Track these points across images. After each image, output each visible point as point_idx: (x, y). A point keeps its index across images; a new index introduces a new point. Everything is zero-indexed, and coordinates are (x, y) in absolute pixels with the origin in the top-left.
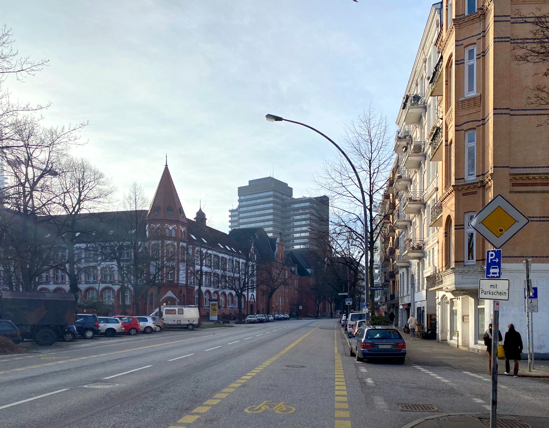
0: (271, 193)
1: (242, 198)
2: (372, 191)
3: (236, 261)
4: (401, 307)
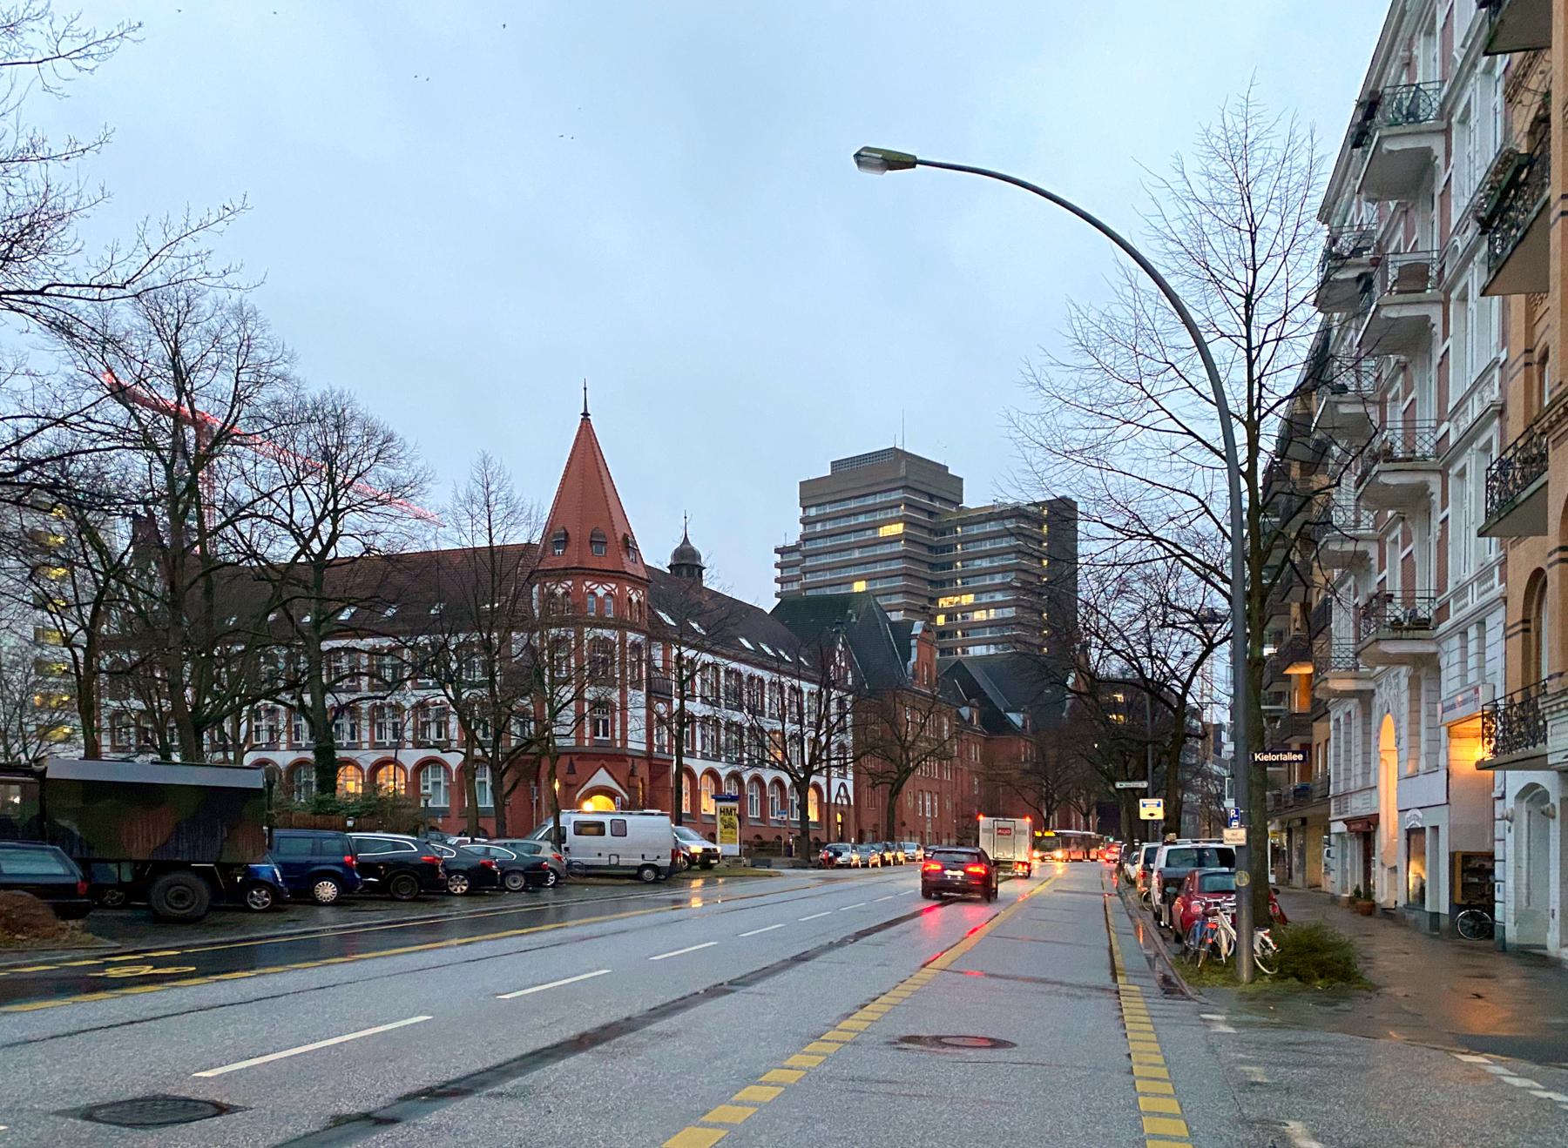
0: (897, 495)
1: (813, 512)
2: (1259, 406)
3: (792, 688)
4: (1338, 827)
